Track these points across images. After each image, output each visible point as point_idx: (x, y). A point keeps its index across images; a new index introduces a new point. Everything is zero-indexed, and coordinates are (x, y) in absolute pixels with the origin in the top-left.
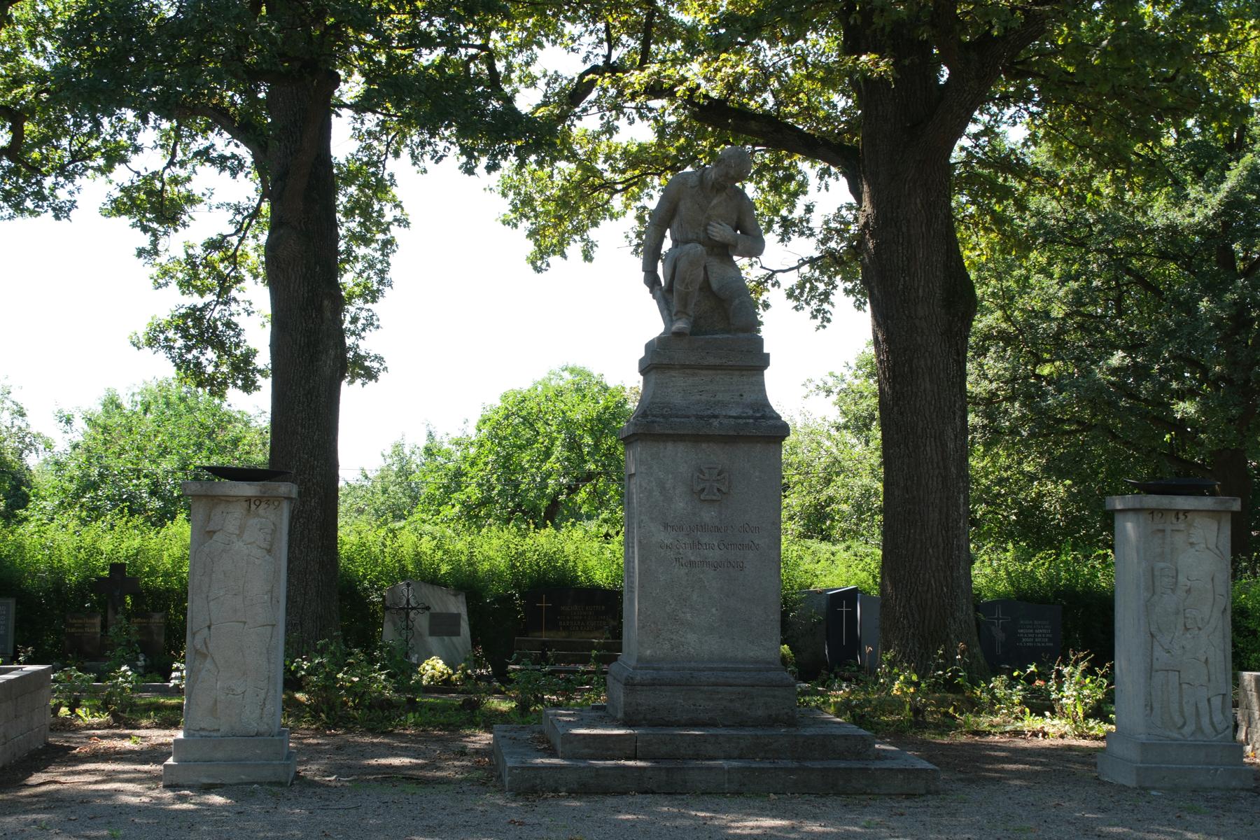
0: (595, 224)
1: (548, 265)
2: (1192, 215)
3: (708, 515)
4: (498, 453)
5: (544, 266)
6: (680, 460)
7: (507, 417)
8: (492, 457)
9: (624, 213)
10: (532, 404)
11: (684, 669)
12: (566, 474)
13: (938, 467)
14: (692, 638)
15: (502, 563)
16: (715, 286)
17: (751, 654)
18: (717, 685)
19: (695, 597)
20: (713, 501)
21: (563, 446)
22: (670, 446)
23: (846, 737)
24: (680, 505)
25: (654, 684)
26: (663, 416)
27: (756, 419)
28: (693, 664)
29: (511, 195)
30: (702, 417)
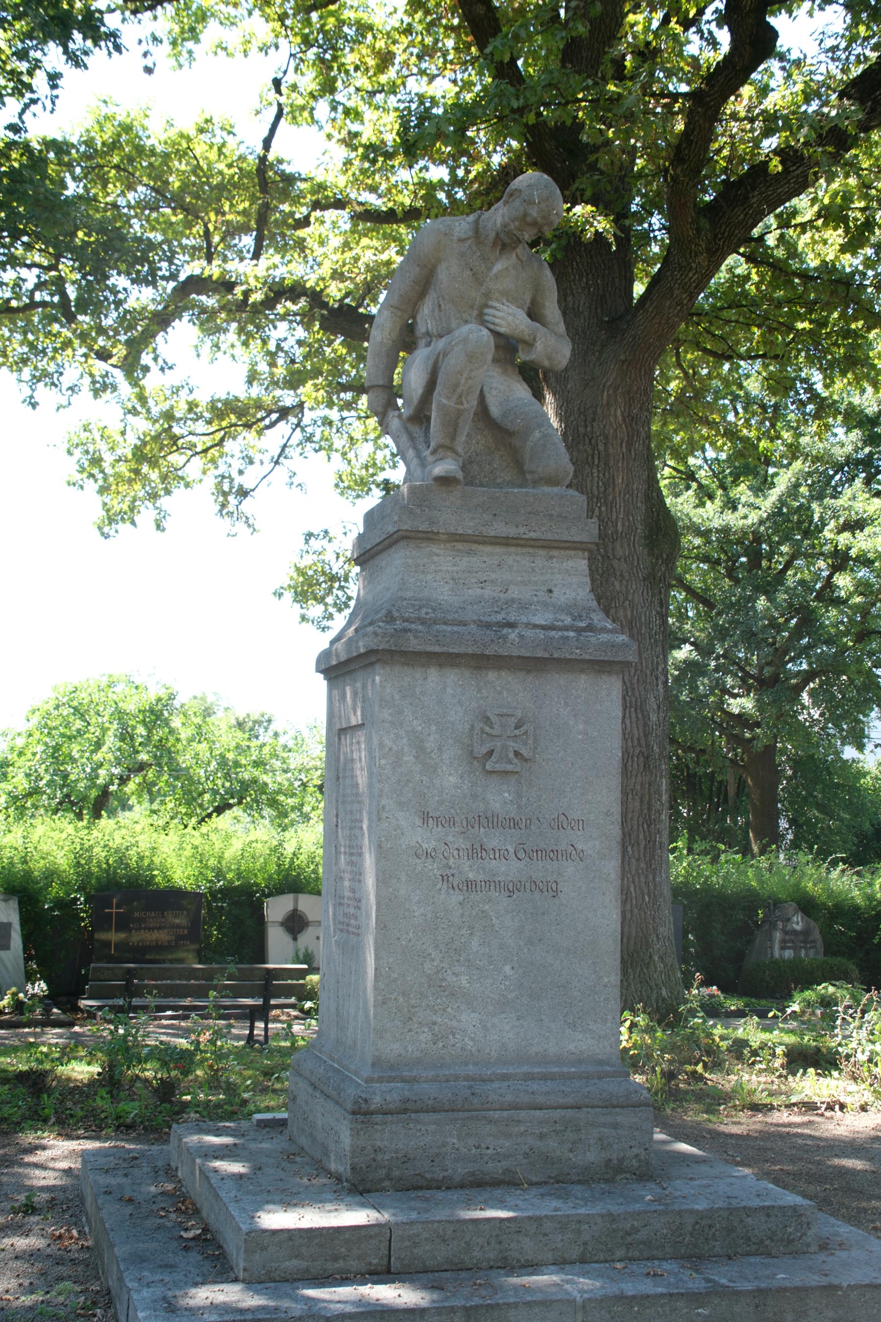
0: (168, 492)
1: (117, 531)
2: (745, 517)
3: (499, 798)
4: (46, 744)
5: (112, 533)
6: (449, 694)
7: (57, 707)
8: (40, 748)
9: (201, 481)
10: (84, 695)
11: (457, 1078)
12: (119, 763)
13: (640, 745)
14: (469, 1019)
15: (62, 860)
16: (495, 411)
17: (571, 1047)
18: (516, 1107)
19: (475, 944)
20: (506, 772)
21: (115, 736)
22: (433, 674)
23: (767, 1211)
24: (451, 779)
25: (406, 1110)
26: (423, 622)
27: (579, 630)
28: (471, 1070)
29: (78, 453)
30: (488, 625)
